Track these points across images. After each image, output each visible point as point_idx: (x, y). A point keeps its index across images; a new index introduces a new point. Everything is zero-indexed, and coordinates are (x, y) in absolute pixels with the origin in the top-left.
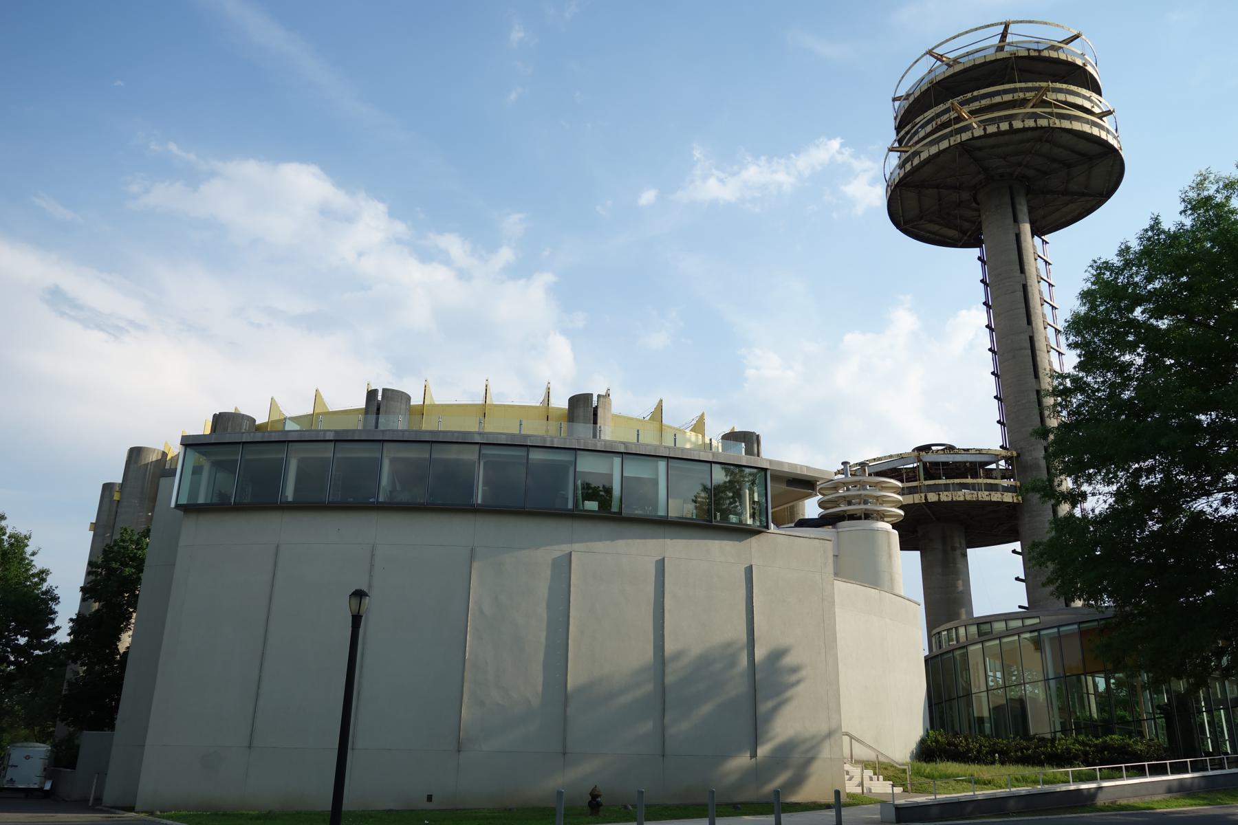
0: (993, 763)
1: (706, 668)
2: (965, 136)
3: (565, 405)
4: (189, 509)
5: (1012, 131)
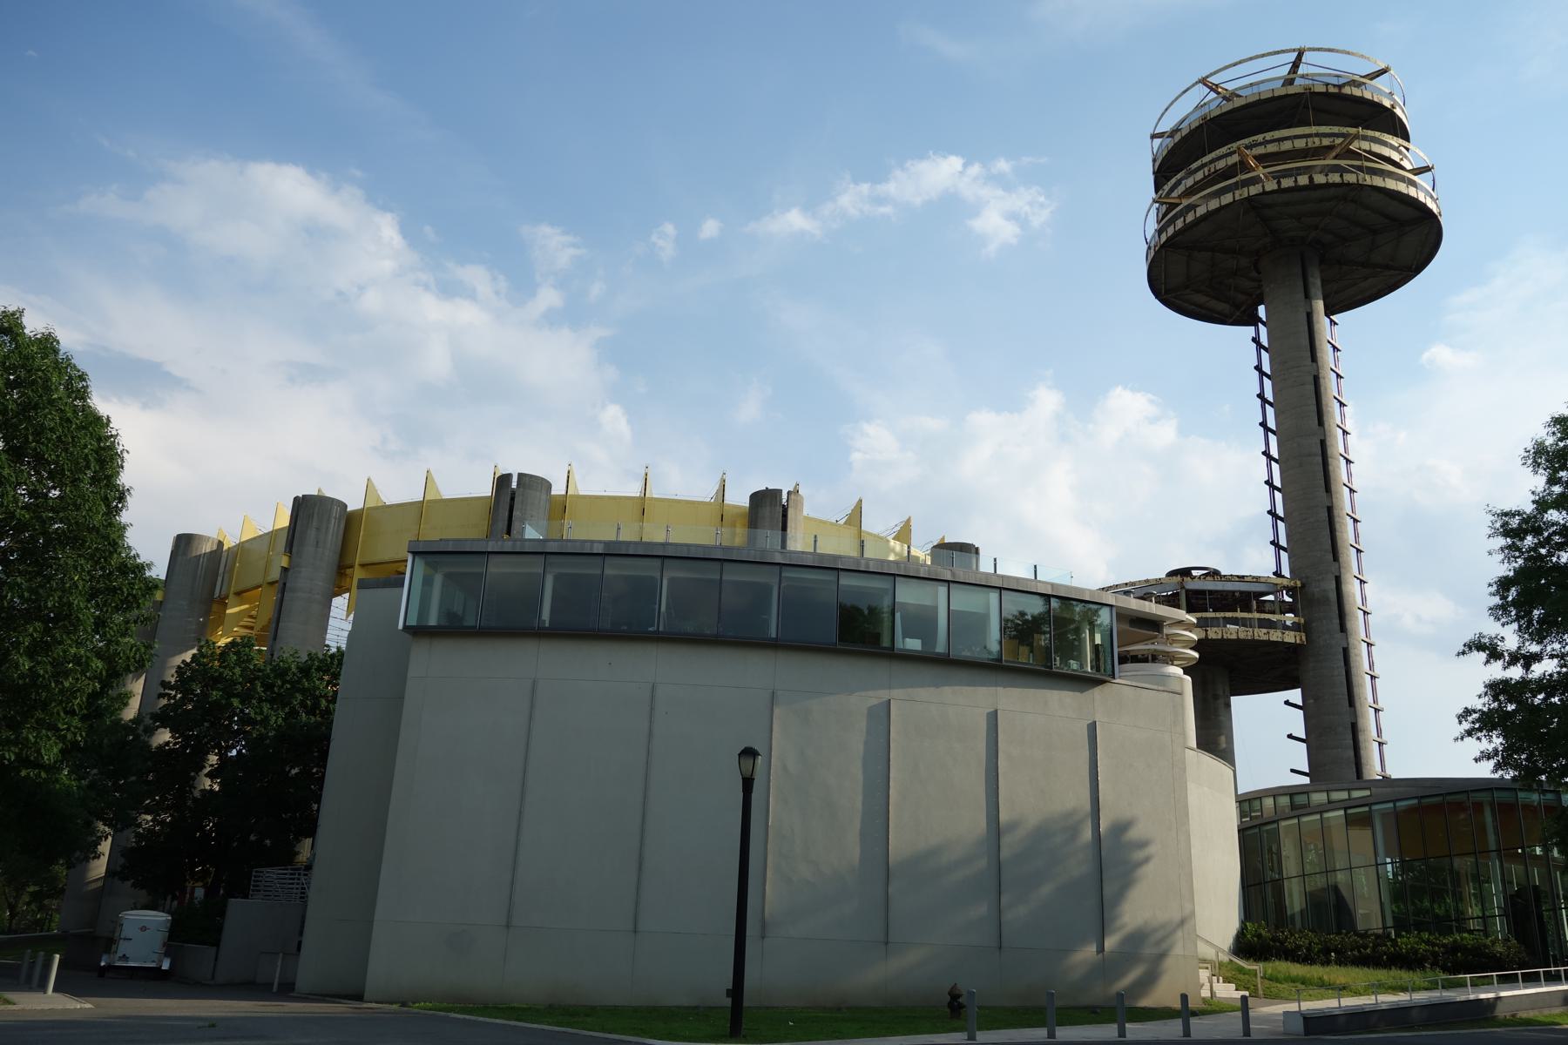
1: (1048, 839)
2: (1254, 190)
3: (746, 502)
4: (418, 632)
5: (1312, 186)
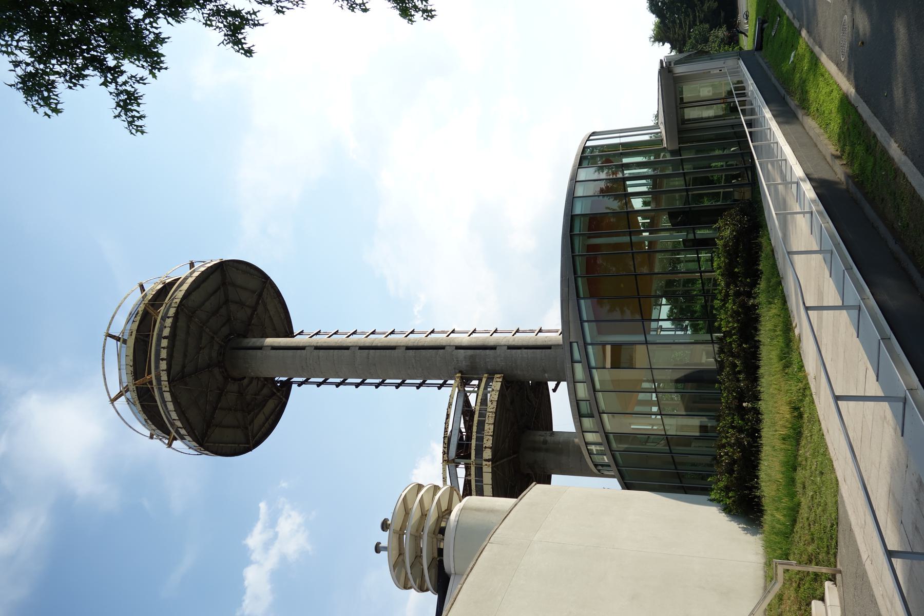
0: (757, 412)
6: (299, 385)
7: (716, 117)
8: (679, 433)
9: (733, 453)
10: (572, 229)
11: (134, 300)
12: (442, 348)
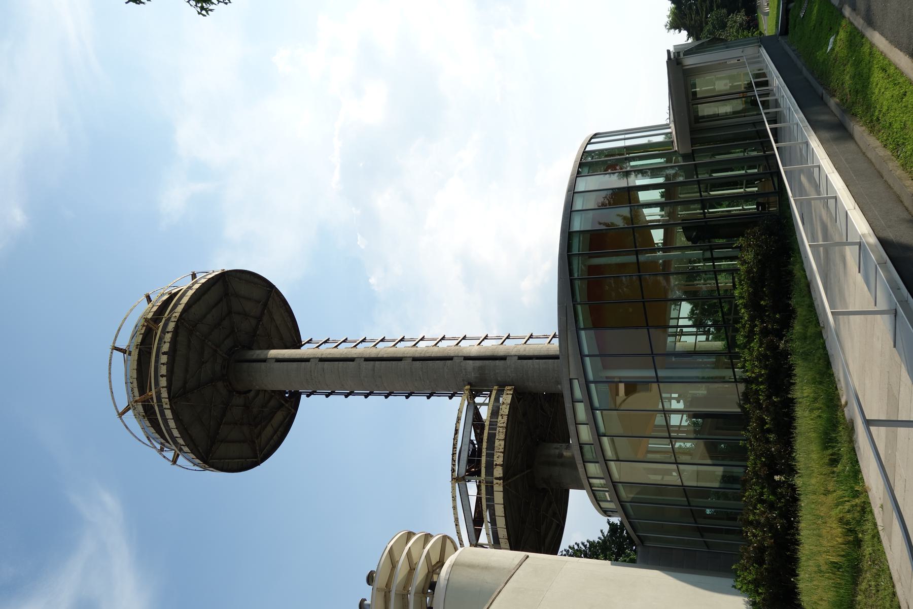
6: (308, 396)
7: (734, 113)
8: (700, 484)
9: (764, 539)
10: (571, 273)
11: (143, 309)
12: (450, 358)
